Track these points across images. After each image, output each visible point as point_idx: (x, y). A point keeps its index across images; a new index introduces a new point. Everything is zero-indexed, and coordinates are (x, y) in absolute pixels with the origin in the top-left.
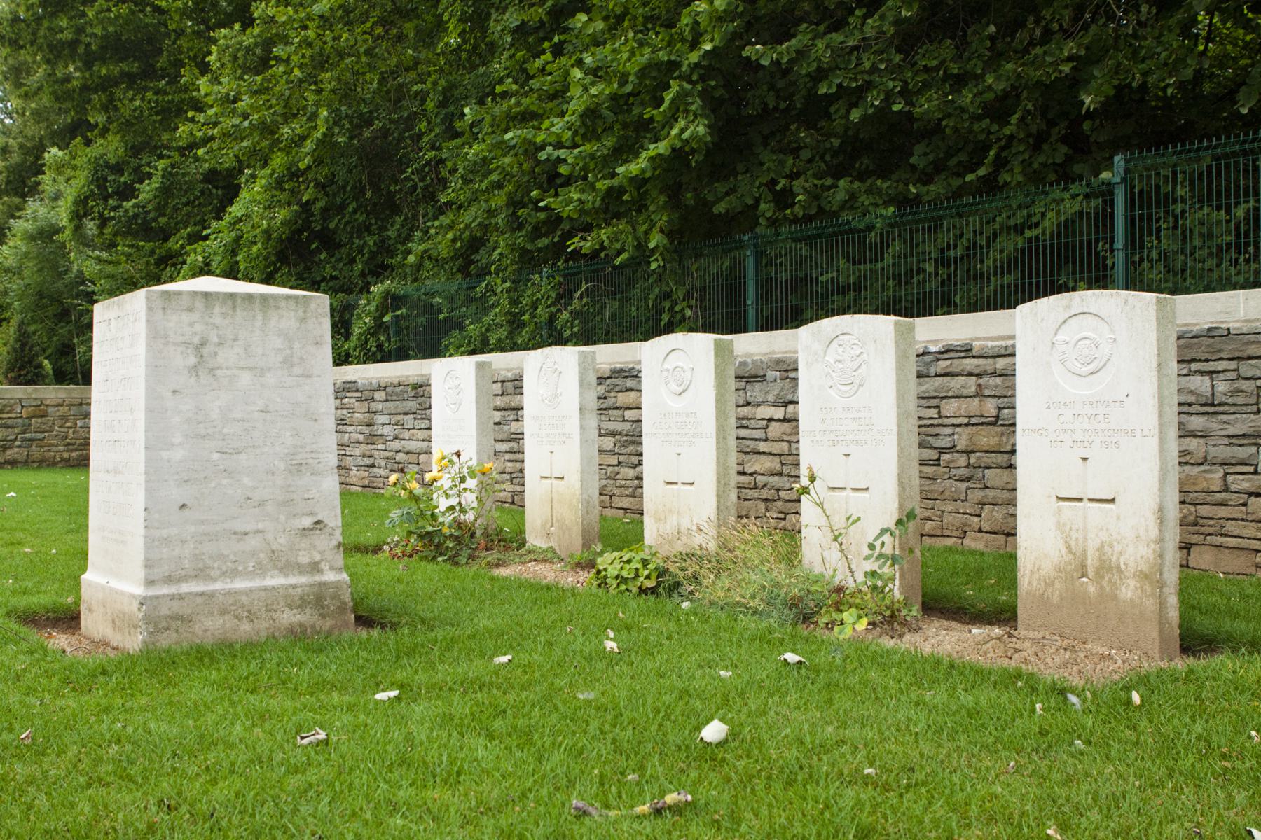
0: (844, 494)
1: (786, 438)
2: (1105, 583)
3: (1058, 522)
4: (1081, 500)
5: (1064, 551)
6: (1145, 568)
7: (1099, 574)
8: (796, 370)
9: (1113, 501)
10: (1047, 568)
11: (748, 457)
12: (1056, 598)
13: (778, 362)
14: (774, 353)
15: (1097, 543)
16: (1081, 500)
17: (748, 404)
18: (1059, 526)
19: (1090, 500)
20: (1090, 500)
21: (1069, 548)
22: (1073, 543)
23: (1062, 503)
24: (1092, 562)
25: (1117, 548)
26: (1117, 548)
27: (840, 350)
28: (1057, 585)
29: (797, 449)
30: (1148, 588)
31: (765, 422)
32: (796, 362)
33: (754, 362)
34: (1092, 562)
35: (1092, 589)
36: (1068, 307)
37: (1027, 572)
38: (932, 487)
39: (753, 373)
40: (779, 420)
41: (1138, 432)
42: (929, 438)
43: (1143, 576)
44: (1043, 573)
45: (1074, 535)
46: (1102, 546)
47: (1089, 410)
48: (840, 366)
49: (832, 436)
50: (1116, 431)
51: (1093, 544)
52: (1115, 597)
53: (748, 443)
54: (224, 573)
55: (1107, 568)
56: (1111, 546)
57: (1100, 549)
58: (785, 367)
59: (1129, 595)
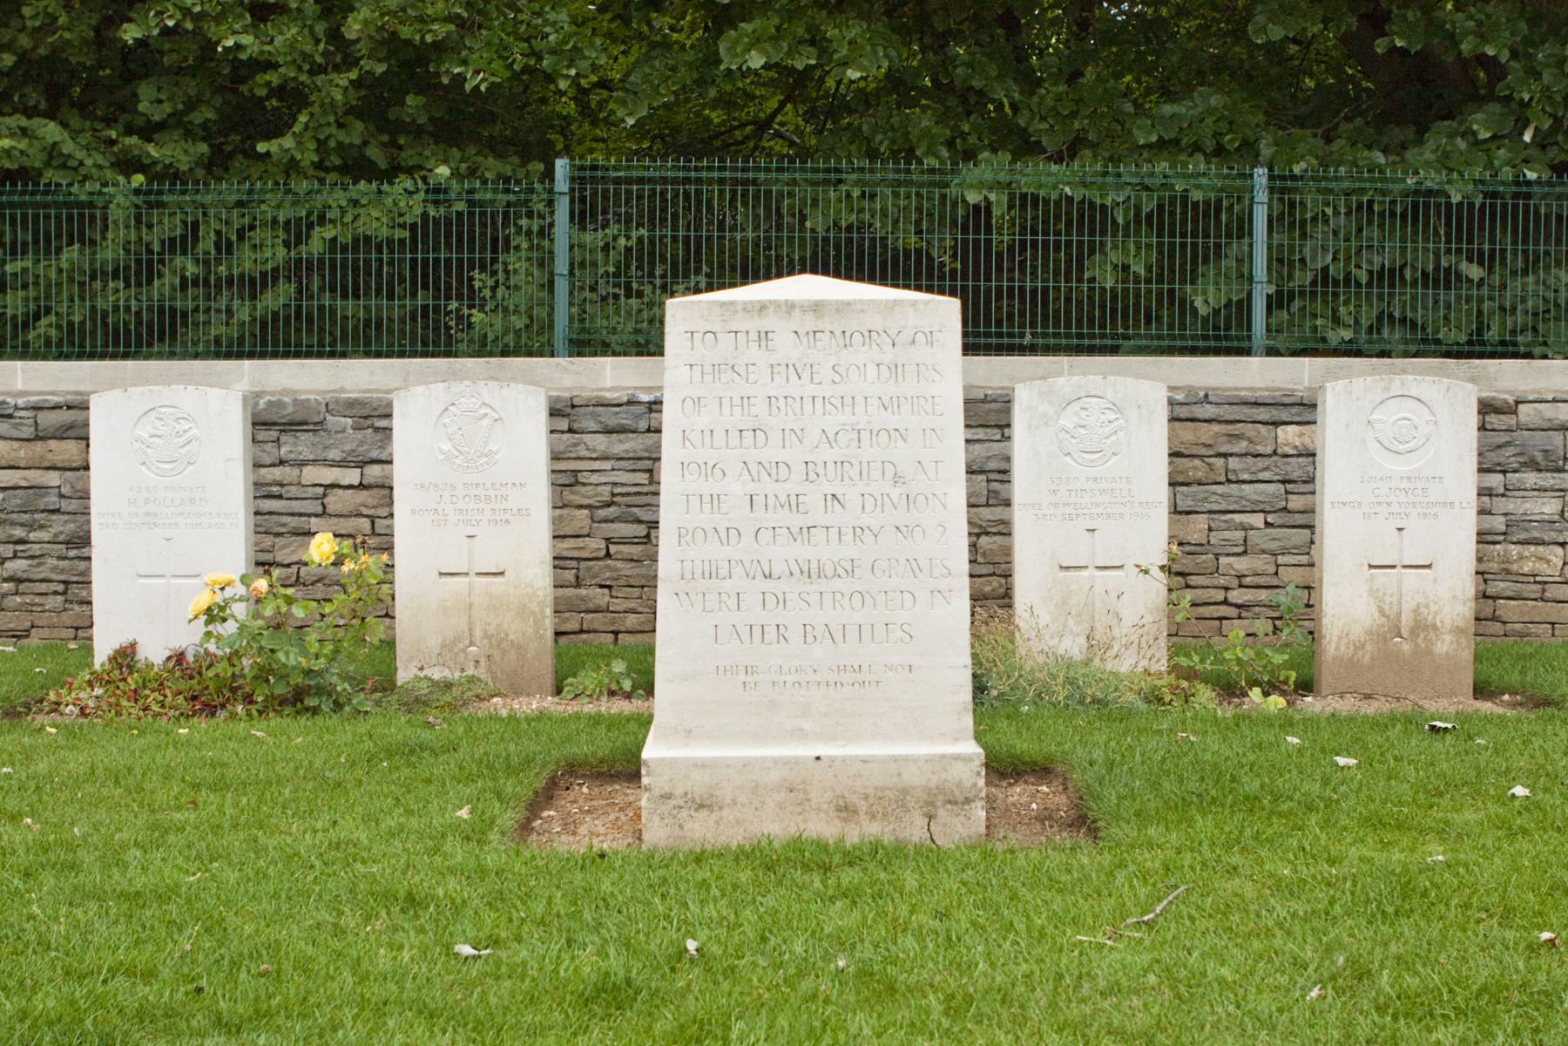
0: (1085, 573)
1: (365, 511)
2: (1420, 641)
3: (1371, 589)
4: (1394, 567)
5: (1377, 615)
6: (1461, 624)
7: (1414, 632)
8: (389, 416)
9: (1429, 566)
10: (1357, 632)
11: (280, 541)
12: (1367, 658)
13: (352, 404)
14: (343, 390)
15: (1413, 605)
16: (1394, 567)
17: (282, 462)
18: (1372, 592)
19: (1405, 567)
20: (1405, 567)
21: (1382, 612)
22: (1386, 607)
23: (444, 579)
24: (1406, 622)
25: (1433, 608)
26: (1433, 608)
27: (1083, 413)
28: (1368, 647)
29: (390, 527)
30: (1463, 641)
31: (320, 490)
32: (390, 405)
33: (296, 402)
34: (1406, 622)
35: (1406, 647)
36: (1387, 389)
37: (1335, 639)
38: (638, 571)
39: (298, 417)
40: (350, 487)
41: (1457, 505)
42: (635, 510)
43: (1458, 631)
44: (1352, 637)
45: (1388, 599)
46: (1418, 607)
47: (1405, 484)
48: (1083, 431)
49: (1069, 510)
50: (1434, 504)
51: (1408, 607)
52: (1430, 652)
53: (285, 519)
54: (943, 735)
55: (1422, 627)
56: (1427, 606)
57: (1416, 611)
58: (366, 412)
59: (1445, 648)
